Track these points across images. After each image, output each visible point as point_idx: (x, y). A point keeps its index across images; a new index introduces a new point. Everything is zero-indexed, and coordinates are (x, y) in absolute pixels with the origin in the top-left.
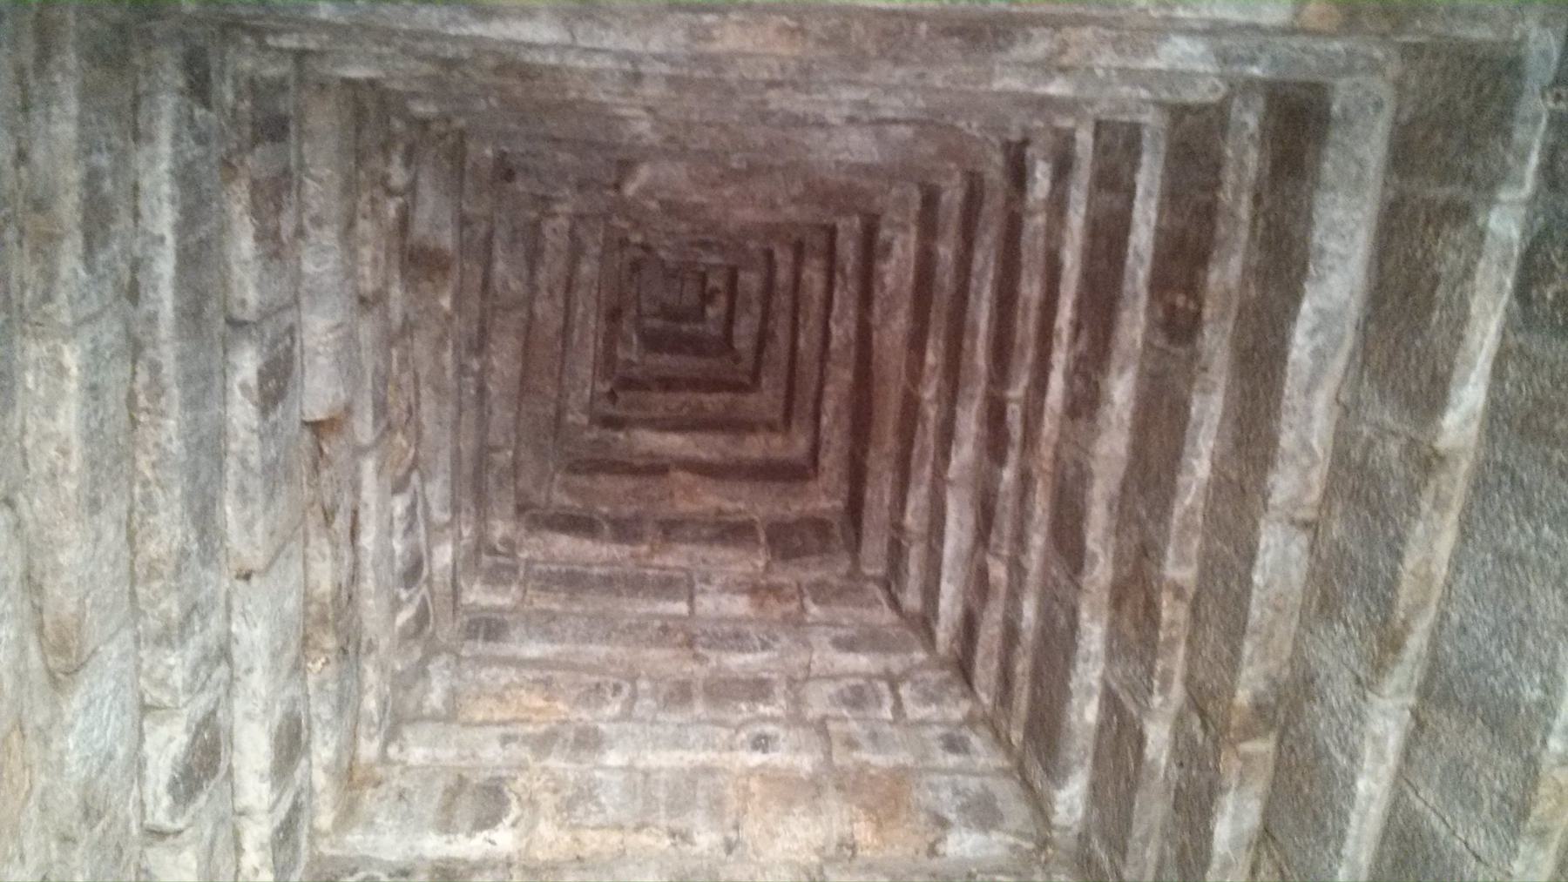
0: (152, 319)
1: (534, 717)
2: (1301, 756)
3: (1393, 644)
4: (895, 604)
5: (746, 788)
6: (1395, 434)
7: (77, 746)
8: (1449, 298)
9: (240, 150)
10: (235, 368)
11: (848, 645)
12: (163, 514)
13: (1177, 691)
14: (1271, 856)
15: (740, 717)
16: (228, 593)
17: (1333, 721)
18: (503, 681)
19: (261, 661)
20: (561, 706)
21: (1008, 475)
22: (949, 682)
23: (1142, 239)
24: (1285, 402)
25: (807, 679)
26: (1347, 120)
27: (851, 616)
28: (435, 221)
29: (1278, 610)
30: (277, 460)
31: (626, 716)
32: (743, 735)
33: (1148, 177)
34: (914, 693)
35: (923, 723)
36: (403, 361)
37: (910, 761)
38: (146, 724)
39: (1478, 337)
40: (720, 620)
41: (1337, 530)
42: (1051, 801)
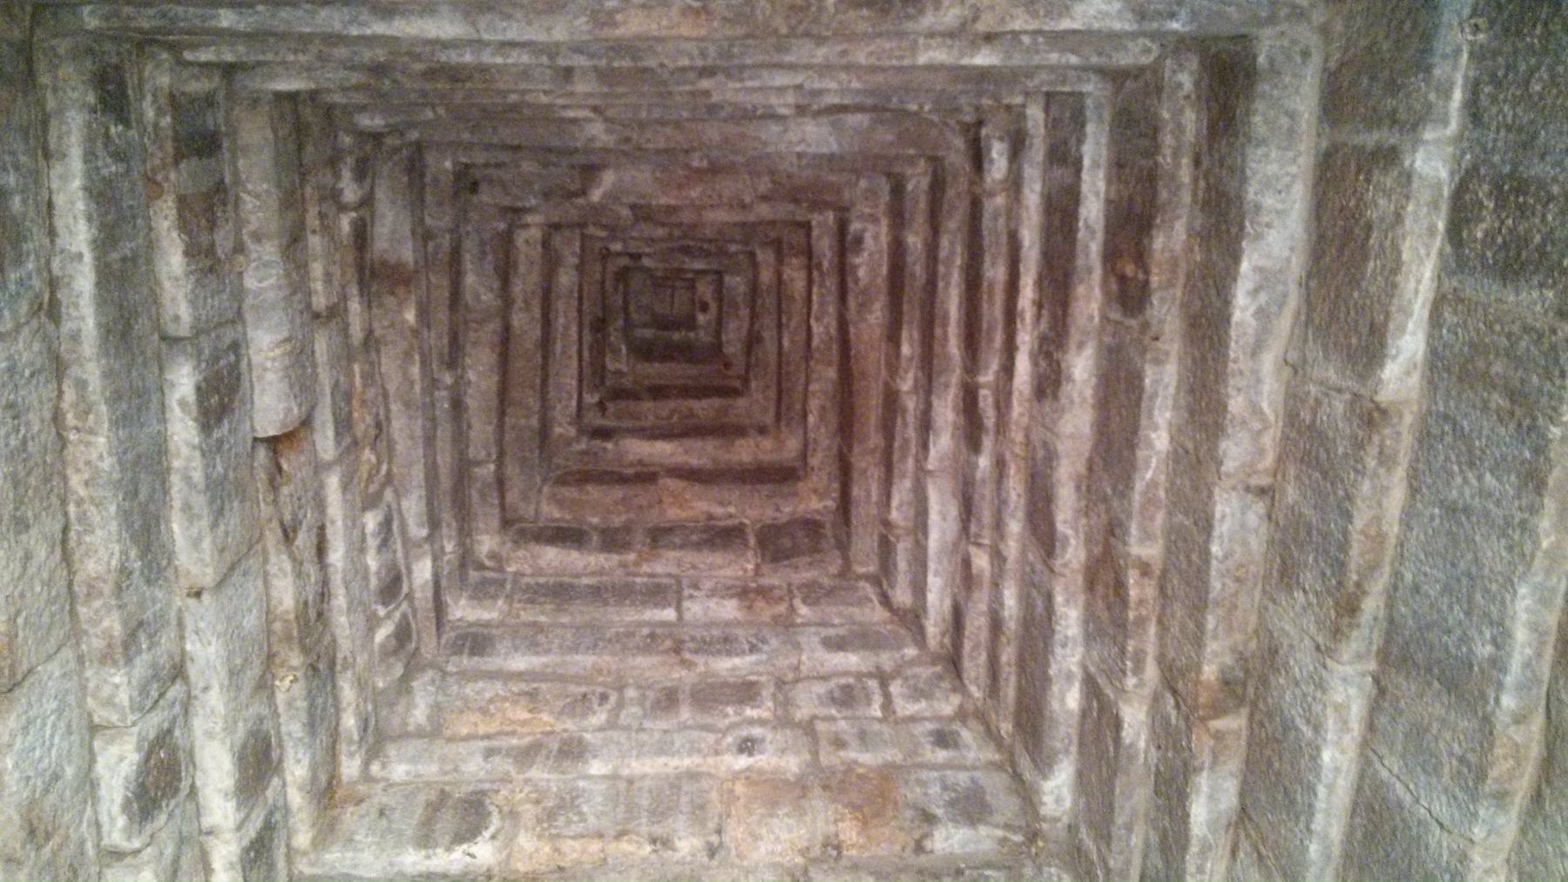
0: (75, 337)
1: (519, 729)
2: (1270, 730)
3: (1350, 608)
4: (886, 601)
5: (731, 791)
6: (1339, 391)
7: (16, 765)
8: (1381, 245)
9: (164, 166)
10: (173, 385)
11: (837, 644)
12: (99, 532)
13: (1151, 671)
14: (1248, 836)
15: (727, 722)
16: (180, 610)
17: (1297, 691)
18: (488, 695)
19: (217, 680)
20: (545, 717)
21: (984, 462)
22: (940, 677)
23: (1092, 210)
24: (1231, 365)
25: (797, 681)
26: (1274, 71)
27: (840, 615)
28: (393, 234)
29: (1238, 580)
30: (225, 476)
31: (611, 725)
32: (730, 739)
33: (1094, 148)
34: (905, 691)
35: (913, 719)
36: (368, 377)
37: (899, 758)
38: (97, 744)
39: (1412, 285)
40: (710, 624)
41: (1291, 493)
42: (1037, 792)
